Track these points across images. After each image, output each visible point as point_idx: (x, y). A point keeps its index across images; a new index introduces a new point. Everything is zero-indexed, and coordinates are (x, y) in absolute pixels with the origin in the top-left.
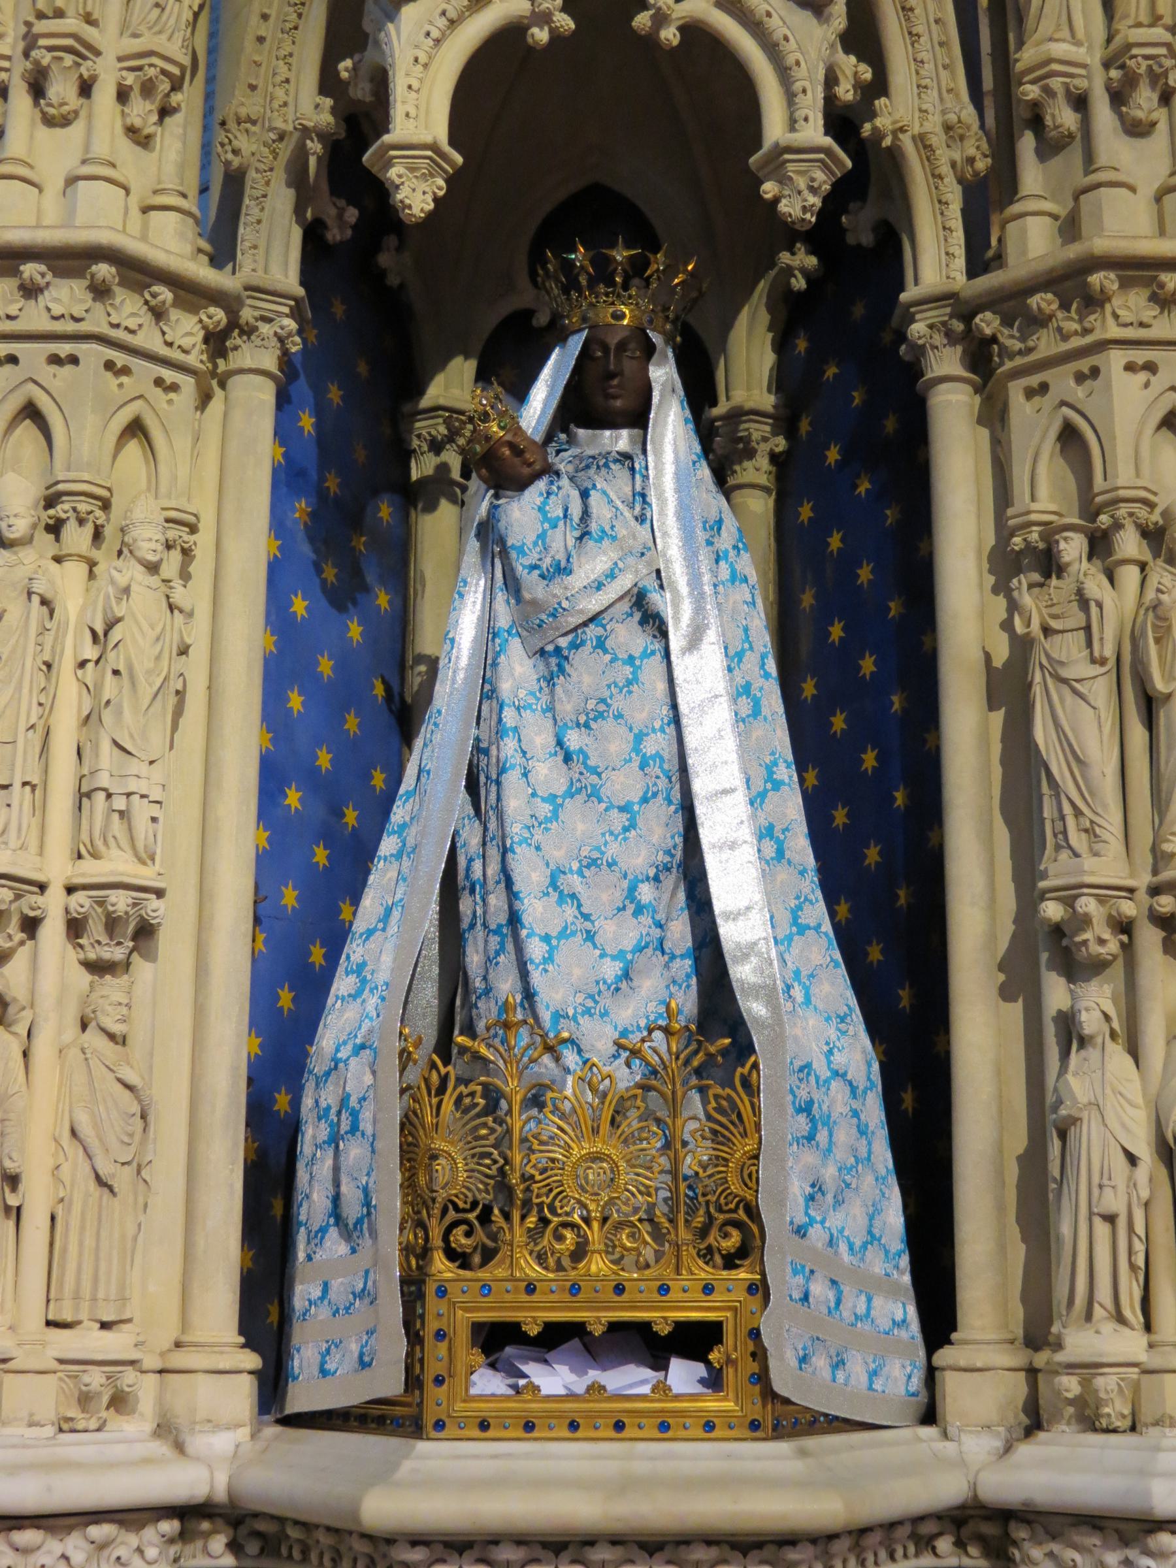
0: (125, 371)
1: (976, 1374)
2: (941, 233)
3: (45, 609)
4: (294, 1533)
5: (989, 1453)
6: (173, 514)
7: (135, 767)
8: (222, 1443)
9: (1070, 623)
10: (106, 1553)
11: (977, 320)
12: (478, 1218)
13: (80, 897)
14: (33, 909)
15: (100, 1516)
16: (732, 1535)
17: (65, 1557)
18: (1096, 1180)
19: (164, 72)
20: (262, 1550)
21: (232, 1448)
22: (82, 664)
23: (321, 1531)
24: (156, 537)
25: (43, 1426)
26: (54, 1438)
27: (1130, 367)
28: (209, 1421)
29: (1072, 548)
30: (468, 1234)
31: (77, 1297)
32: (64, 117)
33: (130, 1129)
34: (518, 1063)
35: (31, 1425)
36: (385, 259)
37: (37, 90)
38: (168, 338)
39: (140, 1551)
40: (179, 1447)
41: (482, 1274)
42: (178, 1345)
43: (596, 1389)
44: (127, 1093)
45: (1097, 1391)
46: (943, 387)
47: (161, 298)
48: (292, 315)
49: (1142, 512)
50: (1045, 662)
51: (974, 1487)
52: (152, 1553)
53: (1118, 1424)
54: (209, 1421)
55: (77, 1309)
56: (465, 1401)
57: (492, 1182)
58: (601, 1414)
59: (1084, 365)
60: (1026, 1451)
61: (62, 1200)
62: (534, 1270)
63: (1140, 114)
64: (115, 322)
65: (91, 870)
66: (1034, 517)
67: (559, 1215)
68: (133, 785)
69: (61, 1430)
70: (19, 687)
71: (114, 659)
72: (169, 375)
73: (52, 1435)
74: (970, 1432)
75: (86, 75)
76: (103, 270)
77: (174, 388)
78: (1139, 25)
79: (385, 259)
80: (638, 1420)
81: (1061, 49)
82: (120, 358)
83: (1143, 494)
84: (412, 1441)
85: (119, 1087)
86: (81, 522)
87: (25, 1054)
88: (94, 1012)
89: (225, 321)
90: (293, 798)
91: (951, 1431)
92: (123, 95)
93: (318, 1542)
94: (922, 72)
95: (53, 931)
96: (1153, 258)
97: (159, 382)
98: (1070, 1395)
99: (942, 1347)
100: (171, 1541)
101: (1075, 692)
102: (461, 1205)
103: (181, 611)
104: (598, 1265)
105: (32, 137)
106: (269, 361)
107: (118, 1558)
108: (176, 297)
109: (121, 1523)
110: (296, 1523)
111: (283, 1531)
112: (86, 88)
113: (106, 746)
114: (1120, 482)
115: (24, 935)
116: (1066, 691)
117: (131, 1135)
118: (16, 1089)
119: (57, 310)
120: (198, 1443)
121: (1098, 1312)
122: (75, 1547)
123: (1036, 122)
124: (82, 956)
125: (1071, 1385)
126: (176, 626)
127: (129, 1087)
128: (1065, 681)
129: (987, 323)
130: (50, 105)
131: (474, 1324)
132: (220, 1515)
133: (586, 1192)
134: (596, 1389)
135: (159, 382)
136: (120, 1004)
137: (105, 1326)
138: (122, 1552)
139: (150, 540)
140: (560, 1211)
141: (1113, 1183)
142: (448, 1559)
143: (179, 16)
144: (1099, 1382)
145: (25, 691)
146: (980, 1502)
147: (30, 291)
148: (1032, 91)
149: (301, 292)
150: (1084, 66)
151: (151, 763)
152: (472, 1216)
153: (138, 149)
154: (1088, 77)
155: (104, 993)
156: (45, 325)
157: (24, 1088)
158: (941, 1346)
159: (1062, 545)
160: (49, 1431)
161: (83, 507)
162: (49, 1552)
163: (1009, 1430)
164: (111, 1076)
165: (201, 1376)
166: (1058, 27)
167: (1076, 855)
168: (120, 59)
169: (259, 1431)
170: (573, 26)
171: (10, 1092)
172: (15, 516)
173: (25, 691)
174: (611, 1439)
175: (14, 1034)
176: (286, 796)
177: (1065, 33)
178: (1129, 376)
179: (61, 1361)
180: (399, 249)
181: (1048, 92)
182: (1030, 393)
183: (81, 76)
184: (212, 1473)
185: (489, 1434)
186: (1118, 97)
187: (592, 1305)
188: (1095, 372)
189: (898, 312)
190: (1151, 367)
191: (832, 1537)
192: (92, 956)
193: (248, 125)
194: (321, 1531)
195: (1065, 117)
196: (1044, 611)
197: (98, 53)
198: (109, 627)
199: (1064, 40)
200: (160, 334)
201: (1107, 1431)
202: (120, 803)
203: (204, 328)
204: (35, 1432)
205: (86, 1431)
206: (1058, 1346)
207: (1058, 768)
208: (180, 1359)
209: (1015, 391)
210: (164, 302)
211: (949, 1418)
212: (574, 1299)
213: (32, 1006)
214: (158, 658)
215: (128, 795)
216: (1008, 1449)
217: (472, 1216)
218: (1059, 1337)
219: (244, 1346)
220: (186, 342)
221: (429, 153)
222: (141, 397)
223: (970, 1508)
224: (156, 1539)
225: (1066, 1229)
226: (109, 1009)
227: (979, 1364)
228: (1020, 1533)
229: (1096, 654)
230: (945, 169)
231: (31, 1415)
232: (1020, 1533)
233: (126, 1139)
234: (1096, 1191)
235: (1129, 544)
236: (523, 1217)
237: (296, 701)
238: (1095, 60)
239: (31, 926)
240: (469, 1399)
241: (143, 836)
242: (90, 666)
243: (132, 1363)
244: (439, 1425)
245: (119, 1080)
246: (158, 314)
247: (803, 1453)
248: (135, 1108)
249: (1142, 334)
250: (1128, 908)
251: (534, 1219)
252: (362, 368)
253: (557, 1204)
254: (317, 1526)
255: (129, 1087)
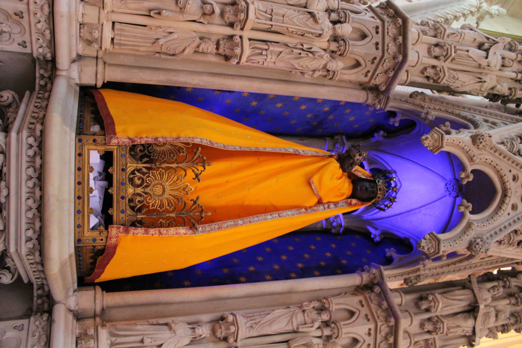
0: (373, 63)
1: (93, 300)
2: (395, 275)
3: (318, 35)
4: (47, 95)
5: (69, 305)
6: (336, 73)
7: (274, 57)
8: (75, 74)
9: (306, 318)
10: (41, 35)
11: (378, 287)
12: (146, 153)
13: (239, 40)
14: (237, 25)
15: (53, 35)
16: (43, 236)
17: (39, 22)
18: (153, 336)
19: (439, 78)
20: (41, 85)
21: (73, 77)
22: (302, 45)
23: (47, 103)
24: (333, 68)
25: (82, 18)
26: (78, 21)
27: (370, 329)
28: (82, 71)
29: (325, 317)
30: (140, 150)
31: (121, 30)
32: (431, 51)
33: (171, 50)
34: (193, 167)
35: (83, 14)
36: (382, 133)
37: (436, 45)
38: (379, 75)
39: (41, 47)
40: (74, 61)
41: (128, 155)
42: (105, 63)
43: (91, 190)
44: (182, 50)
45: (89, 341)
46: (360, 278)
47: (391, 73)
48: (380, 108)
49: (335, 336)
50: (296, 312)
51: (59, 302)
52: (41, 50)
53: (79, 346)
54: (82, 71)
55: (118, 30)
56: (88, 149)
57: (156, 158)
58: (83, 193)
59: (370, 317)
60: (70, 317)
61: (151, 29)
62: (129, 170)
63: (426, 326)
64: (386, 61)
65: (246, 43)
66: (331, 305)
67: (146, 178)
68: (269, 56)
69: (80, 24)
70: (298, 26)
71: (303, 54)
72: (370, 74)
73: (79, 21)
74: (76, 299)
75: (440, 58)
76: (400, 58)
77: (366, 76)
78: (447, 325)
79: (382, 133)
80: (81, 204)
81: (440, 306)
82: (376, 61)
83: (340, 336)
84: (75, 131)
85: (183, 48)
86: (338, 47)
87: (194, 21)
88: (206, 42)
89: (382, 90)
90: (254, 103)
91: (76, 293)
92: (434, 67)
93: (43, 102)
94: (434, 269)
95: (228, 31)
96: (398, 335)
97: (368, 72)
98: (88, 332)
99: (101, 288)
100: (44, 57)
101: (289, 321)
102: (150, 148)
103: (313, 74)
104: (131, 190)
105: (425, 43)
106: (369, 102)
107: (39, 39)
108: (390, 77)
109: (50, 41)
110: (49, 96)
111: (47, 92)
112: (436, 58)
113: (280, 49)
114: (343, 330)
115: (228, 23)
116: (289, 318)
117: (169, 50)
118: (185, 17)
119: (390, 45)
120: (75, 66)
121: (113, 339)
122: (43, 25)
123: (421, 298)
124: (221, 40)
125: (91, 332)
126: (309, 72)
127: (184, 50)
128: (292, 318)
129: (377, 289)
130: (434, 48)
131: (112, 152)
132: (52, 73)
133: (153, 187)
134: (91, 190)
135: (368, 72)
136: (208, 49)
137: (113, 39)
138: (41, 41)
139: (333, 66)
140: (147, 179)
141: (153, 342)
142: (36, 142)
143: (450, 82)
144: (92, 341)
145: (297, 27)
146: (54, 305)
147: (395, 39)
148: (431, 298)
149: (386, 110)
150: (436, 311)
151: (275, 62)
152: (146, 151)
153: (420, 70)
154: (434, 312)
155: (211, 45)
156: (386, 42)
157: (185, 19)
158: (101, 288)
159: (326, 314)
160: (80, 20)
161: (342, 48)
162: (41, 17)
163: (77, 311)
164: (188, 45)
165: (95, 68)
166: (445, 304)
167: (246, 324)
168: (443, 67)
169: (78, 86)
170: (464, 184)
171: (184, 15)
172: (342, 29)
173: (297, 27)
174: (75, 195)
175: (201, 18)
176: (255, 102)
177: (444, 305)
178: (367, 330)
179: (102, 25)
180: (384, 136)
181: (431, 301)
182: (361, 302)
183: (440, 56)
184: (66, 70)
185: (77, 156)
186: (429, 319)
187: (118, 189)
188: (369, 320)
189: (378, 265)
190: (369, 334)
191: (43, 265)
192: (221, 42)
193: (423, 99)
194: (47, 103)
195: (424, 305)
196: (308, 311)
197: (445, 61)
198: (312, 53)
199: (442, 305)
200: (381, 72)
201: (77, 342)
202: (264, 53)
203: (380, 85)
204: (80, 15)
205: (80, 32)
206: (103, 326)
207: (269, 317)
208: (100, 62)
209: (361, 298)
210: (389, 74)
211: (80, 292)
212: (120, 183)
213: (208, 23)
214: (302, 66)
215: (267, 55)
216: (71, 311)
217: (146, 151)
218: (105, 326)
219: (104, 83)
220: (377, 80)
221: (440, 145)
222: (366, 66)
223: (52, 302)
224: (45, 52)
225: (139, 327)
226: (206, 46)
227: (97, 301)
228: (45, 316)
229: (300, 327)
230: (410, 275)
231: (86, 14)
232: (45, 316)
233: (168, 49)
234: (150, 336)
235: (327, 332)
236: (145, 168)
237: (279, 105)
238: (438, 313)
239: (231, 25)
240: (89, 150)
241: (255, 59)
242: (301, 47)
243: (101, 48)
244: (80, 140)
245: (186, 48)
246: (386, 72)
247: (70, 256)
248: (177, 52)
249: (378, 332)
250: (231, 340)
251: (145, 171)
252: (356, 126)
253: (149, 178)
254: (48, 102)
255: (184, 50)
